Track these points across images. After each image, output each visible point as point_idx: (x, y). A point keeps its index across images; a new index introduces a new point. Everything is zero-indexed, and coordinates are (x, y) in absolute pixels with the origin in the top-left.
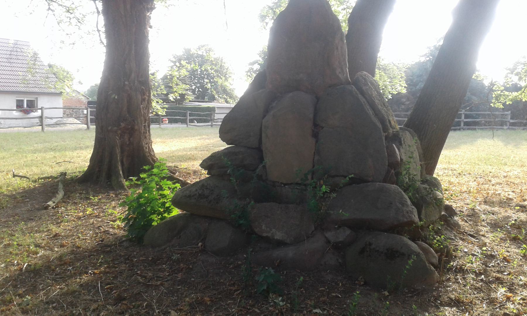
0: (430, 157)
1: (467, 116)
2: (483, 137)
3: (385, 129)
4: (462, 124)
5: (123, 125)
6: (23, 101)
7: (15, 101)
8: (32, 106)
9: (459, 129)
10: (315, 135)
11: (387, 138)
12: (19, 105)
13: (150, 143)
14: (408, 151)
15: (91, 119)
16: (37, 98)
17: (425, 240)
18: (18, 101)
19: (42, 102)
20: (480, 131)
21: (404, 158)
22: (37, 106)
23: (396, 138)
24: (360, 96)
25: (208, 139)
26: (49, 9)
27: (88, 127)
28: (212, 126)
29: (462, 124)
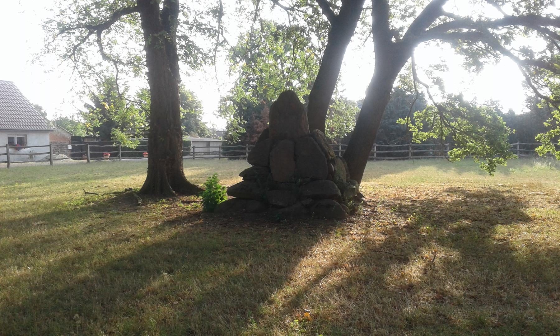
0: (356, 175)
1: (378, 148)
2: (423, 165)
3: (327, 156)
4: (410, 155)
5: (168, 157)
6: (13, 137)
7: (7, 138)
8: (22, 143)
9: (407, 159)
10: (295, 160)
11: (328, 161)
12: (11, 141)
13: (182, 169)
14: (341, 169)
15: (90, 154)
16: (26, 135)
17: (344, 203)
18: (10, 138)
19: (32, 140)
20: (423, 160)
21: (336, 169)
22: (27, 143)
23: (333, 161)
24: (315, 142)
25: (200, 169)
26: (75, 66)
27: (88, 161)
28: (193, 158)
29: (375, 155)
